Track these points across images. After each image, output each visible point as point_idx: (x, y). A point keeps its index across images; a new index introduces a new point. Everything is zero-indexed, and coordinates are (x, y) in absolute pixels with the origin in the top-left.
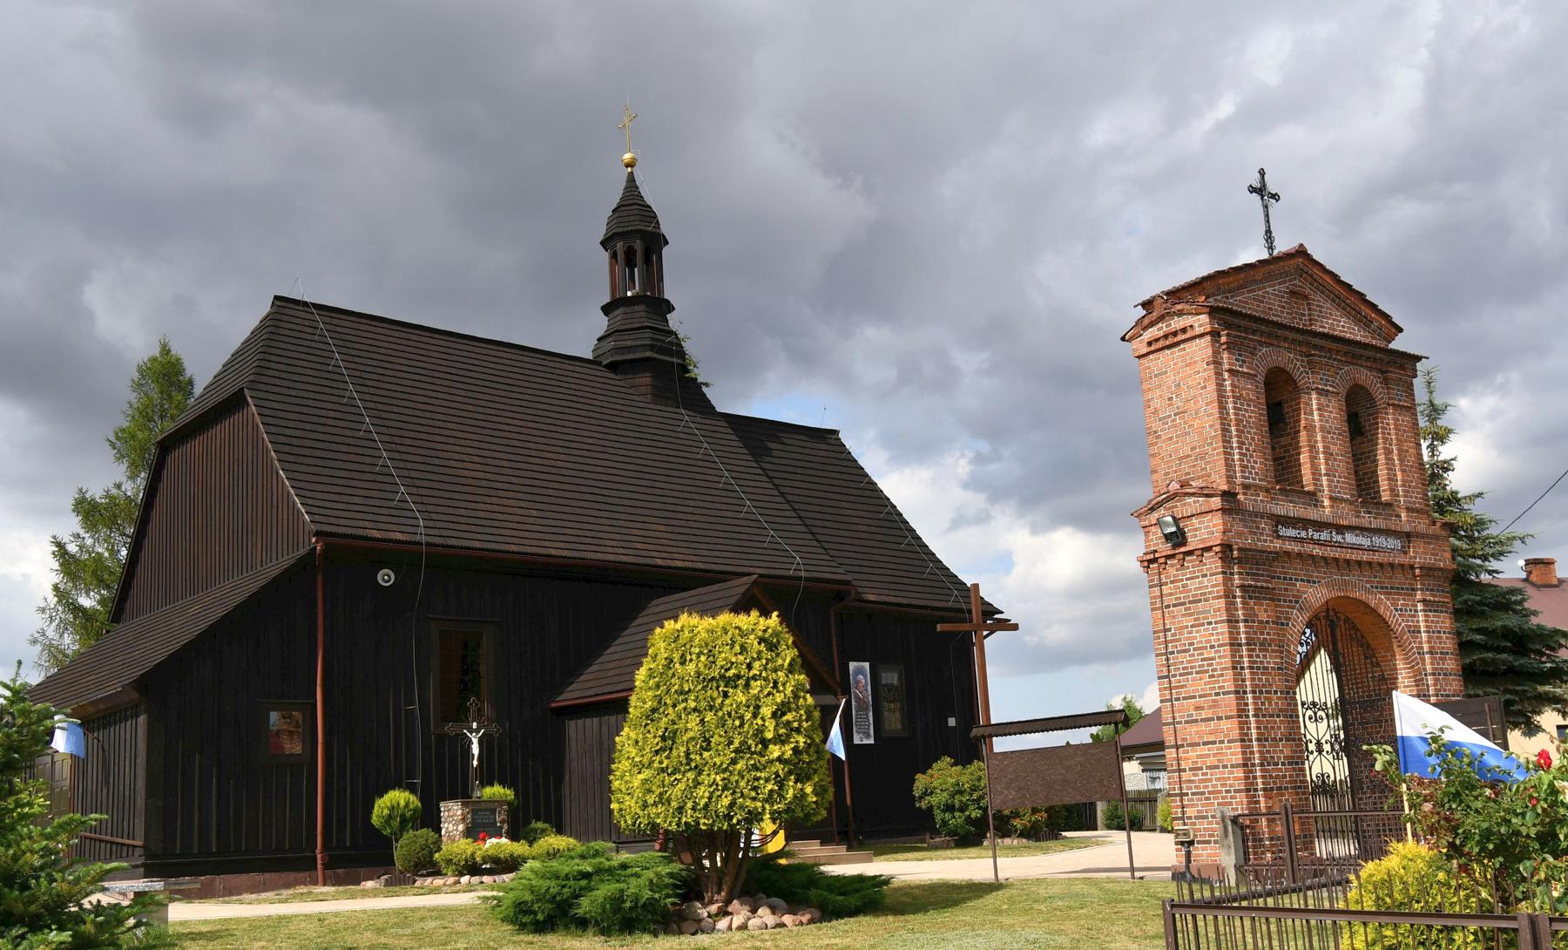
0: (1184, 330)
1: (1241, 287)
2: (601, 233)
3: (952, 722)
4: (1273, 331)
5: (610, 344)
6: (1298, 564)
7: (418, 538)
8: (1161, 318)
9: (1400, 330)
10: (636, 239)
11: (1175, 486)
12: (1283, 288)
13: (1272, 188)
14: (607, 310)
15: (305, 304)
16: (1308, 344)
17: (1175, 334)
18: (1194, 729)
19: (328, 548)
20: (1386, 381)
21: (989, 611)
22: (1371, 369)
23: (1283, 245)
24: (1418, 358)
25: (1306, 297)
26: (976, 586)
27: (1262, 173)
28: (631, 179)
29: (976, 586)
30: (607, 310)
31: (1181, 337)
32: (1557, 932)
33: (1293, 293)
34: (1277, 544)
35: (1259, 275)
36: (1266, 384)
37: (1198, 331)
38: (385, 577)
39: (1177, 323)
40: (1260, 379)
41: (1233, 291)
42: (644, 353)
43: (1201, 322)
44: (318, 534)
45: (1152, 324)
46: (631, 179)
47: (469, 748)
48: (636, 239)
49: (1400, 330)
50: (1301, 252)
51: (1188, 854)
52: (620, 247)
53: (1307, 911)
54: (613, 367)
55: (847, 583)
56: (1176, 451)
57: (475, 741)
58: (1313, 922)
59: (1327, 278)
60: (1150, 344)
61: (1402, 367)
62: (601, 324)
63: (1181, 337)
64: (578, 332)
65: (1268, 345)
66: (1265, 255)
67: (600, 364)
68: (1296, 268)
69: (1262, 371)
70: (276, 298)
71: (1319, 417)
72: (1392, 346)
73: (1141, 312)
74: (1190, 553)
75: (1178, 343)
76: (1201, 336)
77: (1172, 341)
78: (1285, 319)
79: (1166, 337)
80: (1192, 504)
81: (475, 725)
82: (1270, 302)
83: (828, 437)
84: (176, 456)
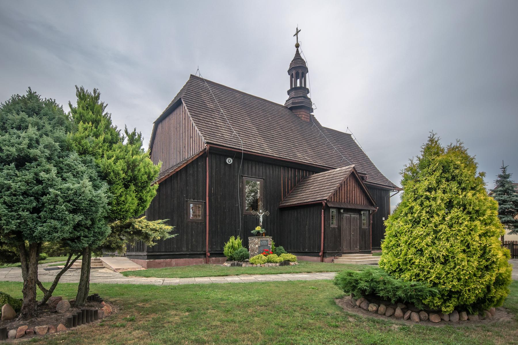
2: (288, 68)
5: (291, 101)
7: (240, 148)
10: (298, 69)
15: (202, 80)
19: (211, 148)
28: (298, 53)
38: (229, 161)
42: (300, 102)
44: (207, 143)
46: (298, 53)
47: (259, 219)
52: (294, 72)
54: (291, 109)
57: (261, 217)
58: (184, 249)
64: (280, 96)
67: (287, 107)
70: (191, 75)
81: (261, 211)
83: (350, 135)
84: (160, 126)
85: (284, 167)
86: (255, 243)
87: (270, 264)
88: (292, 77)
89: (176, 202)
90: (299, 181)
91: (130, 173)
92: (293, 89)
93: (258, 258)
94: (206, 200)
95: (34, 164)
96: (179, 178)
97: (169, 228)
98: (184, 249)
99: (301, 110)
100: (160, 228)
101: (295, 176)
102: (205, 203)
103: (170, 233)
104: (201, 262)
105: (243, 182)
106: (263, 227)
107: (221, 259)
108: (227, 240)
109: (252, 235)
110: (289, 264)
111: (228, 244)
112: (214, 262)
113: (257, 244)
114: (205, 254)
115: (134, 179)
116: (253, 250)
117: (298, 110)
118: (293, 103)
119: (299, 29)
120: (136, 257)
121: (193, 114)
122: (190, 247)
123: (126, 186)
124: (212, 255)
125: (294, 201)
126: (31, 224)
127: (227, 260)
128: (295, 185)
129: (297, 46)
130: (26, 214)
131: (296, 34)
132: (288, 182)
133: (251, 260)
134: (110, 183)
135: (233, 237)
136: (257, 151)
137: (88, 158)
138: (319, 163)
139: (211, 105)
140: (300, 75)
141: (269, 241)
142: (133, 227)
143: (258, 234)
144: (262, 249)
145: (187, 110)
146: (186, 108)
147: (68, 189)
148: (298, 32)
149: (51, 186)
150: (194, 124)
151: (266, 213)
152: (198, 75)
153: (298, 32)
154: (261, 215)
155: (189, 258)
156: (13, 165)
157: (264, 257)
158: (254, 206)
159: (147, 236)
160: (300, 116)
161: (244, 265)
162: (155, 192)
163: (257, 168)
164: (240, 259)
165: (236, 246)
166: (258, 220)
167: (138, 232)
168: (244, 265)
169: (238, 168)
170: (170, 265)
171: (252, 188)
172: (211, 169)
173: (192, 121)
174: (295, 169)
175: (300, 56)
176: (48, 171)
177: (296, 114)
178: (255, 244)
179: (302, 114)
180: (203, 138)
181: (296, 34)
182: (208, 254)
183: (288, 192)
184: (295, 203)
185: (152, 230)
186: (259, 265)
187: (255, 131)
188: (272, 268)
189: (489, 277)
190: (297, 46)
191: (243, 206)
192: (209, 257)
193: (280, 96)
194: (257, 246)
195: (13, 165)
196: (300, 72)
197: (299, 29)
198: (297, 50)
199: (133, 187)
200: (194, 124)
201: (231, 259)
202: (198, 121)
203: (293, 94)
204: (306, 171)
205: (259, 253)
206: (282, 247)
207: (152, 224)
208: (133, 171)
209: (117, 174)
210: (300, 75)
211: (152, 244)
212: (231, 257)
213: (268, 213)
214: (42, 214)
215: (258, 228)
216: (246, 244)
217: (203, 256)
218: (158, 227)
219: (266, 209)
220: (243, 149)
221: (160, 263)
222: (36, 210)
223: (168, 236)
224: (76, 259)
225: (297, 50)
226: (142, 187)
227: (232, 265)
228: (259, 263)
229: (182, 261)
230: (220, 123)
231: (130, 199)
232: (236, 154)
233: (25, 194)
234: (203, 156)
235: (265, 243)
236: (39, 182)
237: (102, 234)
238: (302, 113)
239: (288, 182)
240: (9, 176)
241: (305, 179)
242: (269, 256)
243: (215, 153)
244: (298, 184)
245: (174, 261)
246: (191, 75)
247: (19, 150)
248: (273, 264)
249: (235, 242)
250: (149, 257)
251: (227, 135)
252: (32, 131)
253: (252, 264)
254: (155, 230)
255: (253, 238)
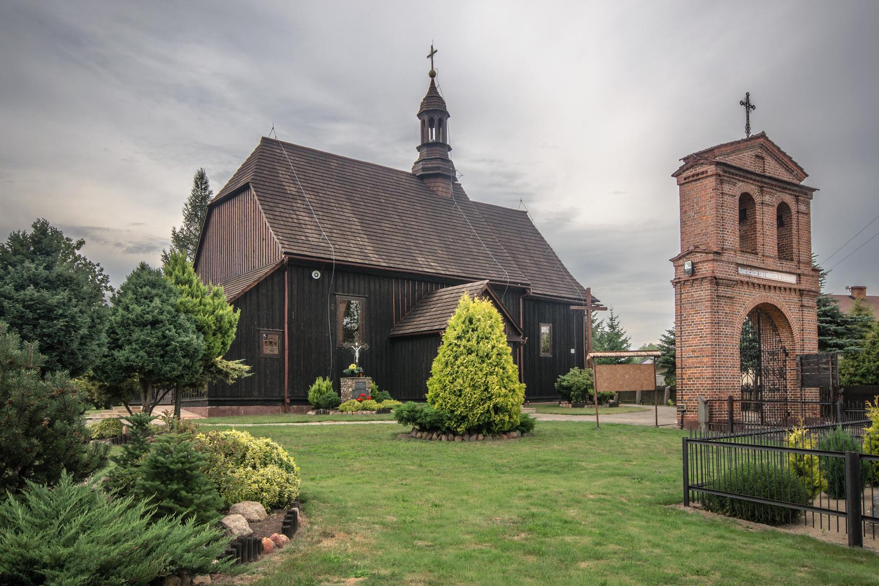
0: (702, 173)
1: (733, 152)
2: (418, 110)
3: (573, 351)
4: (744, 174)
6: (746, 287)
7: (332, 257)
8: (692, 167)
9: (807, 176)
10: (434, 112)
11: (692, 248)
12: (752, 153)
13: (752, 103)
14: (419, 149)
16: (762, 182)
17: (698, 175)
18: (690, 361)
20: (797, 201)
21: (594, 300)
22: (791, 194)
23: (754, 132)
24: (814, 190)
25: (763, 158)
26: (589, 289)
27: (748, 95)
28: (433, 87)
29: (589, 289)
30: (419, 149)
31: (700, 176)
32: (46, 268)
33: (757, 156)
34: (737, 278)
35: (742, 146)
36: (740, 200)
37: (709, 173)
38: (316, 275)
39: (699, 169)
40: (737, 198)
41: (728, 154)
43: (711, 169)
44: (286, 253)
45: (687, 169)
46: (433, 87)
48: (434, 112)
49: (807, 176)
50: (763, 135)
51: (682, 417)
52: (426, 118)
53: (748, 445)
54: (421, 177)
55: (529, 285)
56: (694, 231)
58: (256, 393)
59: (775, 149)
60: (685, 179)
61: (806, 194)
62: (416, 156)
63: (700, 176)
64: (405, 158)
65: (743, 181)
66: (745, 137)
68: (762, 144)
69: (738, 194)
70: (263, 138)
71: (766, 217)
72: (801, 183)
73: (683, 163)
74: (696, 280)
75: (699, 179)
76: (712, 175)
77: (697, 178)
78: (751, 169)
79: (693, 176)
80: (699, 257)
82: (746, 160)
84: (216, 211)
85: (397, 279)
86: (348, 385)
87: (364, 412)
88: (423, 123)
89: (244, 331)
90: (420, 298)
91: (218, 325)
92: (425, 145)
93: (350, 404)
94: (284, 328)
95: (160, 325)
96: (248, 301)
97: (247, 368)
98: (256, 393)
99: (436, 180)
100: (238, 368)
101: (414, 291)
102: (283, 332)
103: (247, 372)
104: (278, 411)
105: (335, 303)
106: (360, 364)
107: (305, 407)
108: (313, 382)
109: (346, 376)
110: (389, 412)
111: (315, 387)
112: (296, 412)
113: (351, 387)
114: (283, 401)
115: (220, 328)
116: (346, 396)
117: (432, 180)
118: (423, 169)
119: (435, 49)
120: (771, 148)
121: (266, 207)
122: (263, 391)
123: (214, 335)
124: (293, 402)
125: (409, 329)
126: (160, 366)
127: (313, 409)
128: (414, 304)
129: (433, 75)
130: (158, 359)
131: (431, 56)
132: (403, 301)
133: (341, 407)
134: (204, 333)
135: (321, 378)
136: (355, 259)
137: (190, 315)
138: (453, 271)
139: (291, 189)
140: (436, 122)
141: (369, 384)
142: (216, 367)
143: (352, 374)
144: (357, 393)
145: (258, 202)
146: (256, 198)
147: (183, 342)
148: (433, 52)
149: (173, 340)
150: (268, 224)
151: (364, 346)
152: (272, 137)
153: (433, 52)
154: (357, 349)
155: (261, 405)
156: (149, 327)
157: (357, 403)
158: (349, 335)
159: (227, 375)
160: (435, 189)
161: (331, 413)
162: (234, 336)
163: (357, 282)
164: (329, 405)
165: (324, 389)
166: (353, 356)
167: (220, 371)
168: (331, 413)
169: (329, 282)
170: (238, 414)
171: (351, 313)
172: (292, 285)
173: (265, 219)
174: (414, 281)
175: (437, 93)
176: (170, 330)
177: (429, 185)
178: (349, 388)
179: (441, 188)
180: (280, 246)
181: (431, 56)
182: (288, 401)
183: (403, 314)
184: (425, 329)
185: (232, 369)
186: (350, 412)
187: (357, 226)
188: (366, 415)
189: (490, 404)
190: (433, 75)
191: (334, 334)
192: (290, 404)
193: (405, 158)
194: (350, 390)
195: (149, 327)
196: (436, 118)
197: (435, 49)
198: (433, 82)
199: (219, 335)
200: (268, 224)
201: (317, 407)
202: (273, 220)
203: (425, 150)
204: (432, 283)
205: (352, 398)
206: (386, 392)
207: (232, 364)
208: (220, 322)
209: (210, 327)
210: (436, 122)
211: (231, 382)
212: (318, 404)
213: (366, 346)
214: (166, 359)
215: (353, 367)
216: (337, 387)
217: (280, 404)
218: (237, 366)
219: (363, 340)
220: (334, 257)
221: (224, 411)
222: (162, 356)
223: (246, 375)
224: (164, 394)
225: (433, 82)
226: (225, 333)
227: (317, 413)
228: (350, 409)
229: (253, 408)
230: (304, 217)
231: (217, 345)
232: (324, 266)
233: (157, 346)
234: (281, 269)
235: (361, 386)
236: (164, 337)
237: (197, 372)
238: (437, 184)
239: (403, 301)
240: (148, 335)
241: (430, 294)
242: (365, 402)
243: (296, 265)
244: (419, 302)
245: (242, 409)
246: (263, 138)
247: (153, 317)
248: (369, 412)
249: (322, 384)
250: (211, 403)
251: (313, 238)
252: (157, 301)
253: (342, 411)
254: (235, 370)
255: (345, 379)
